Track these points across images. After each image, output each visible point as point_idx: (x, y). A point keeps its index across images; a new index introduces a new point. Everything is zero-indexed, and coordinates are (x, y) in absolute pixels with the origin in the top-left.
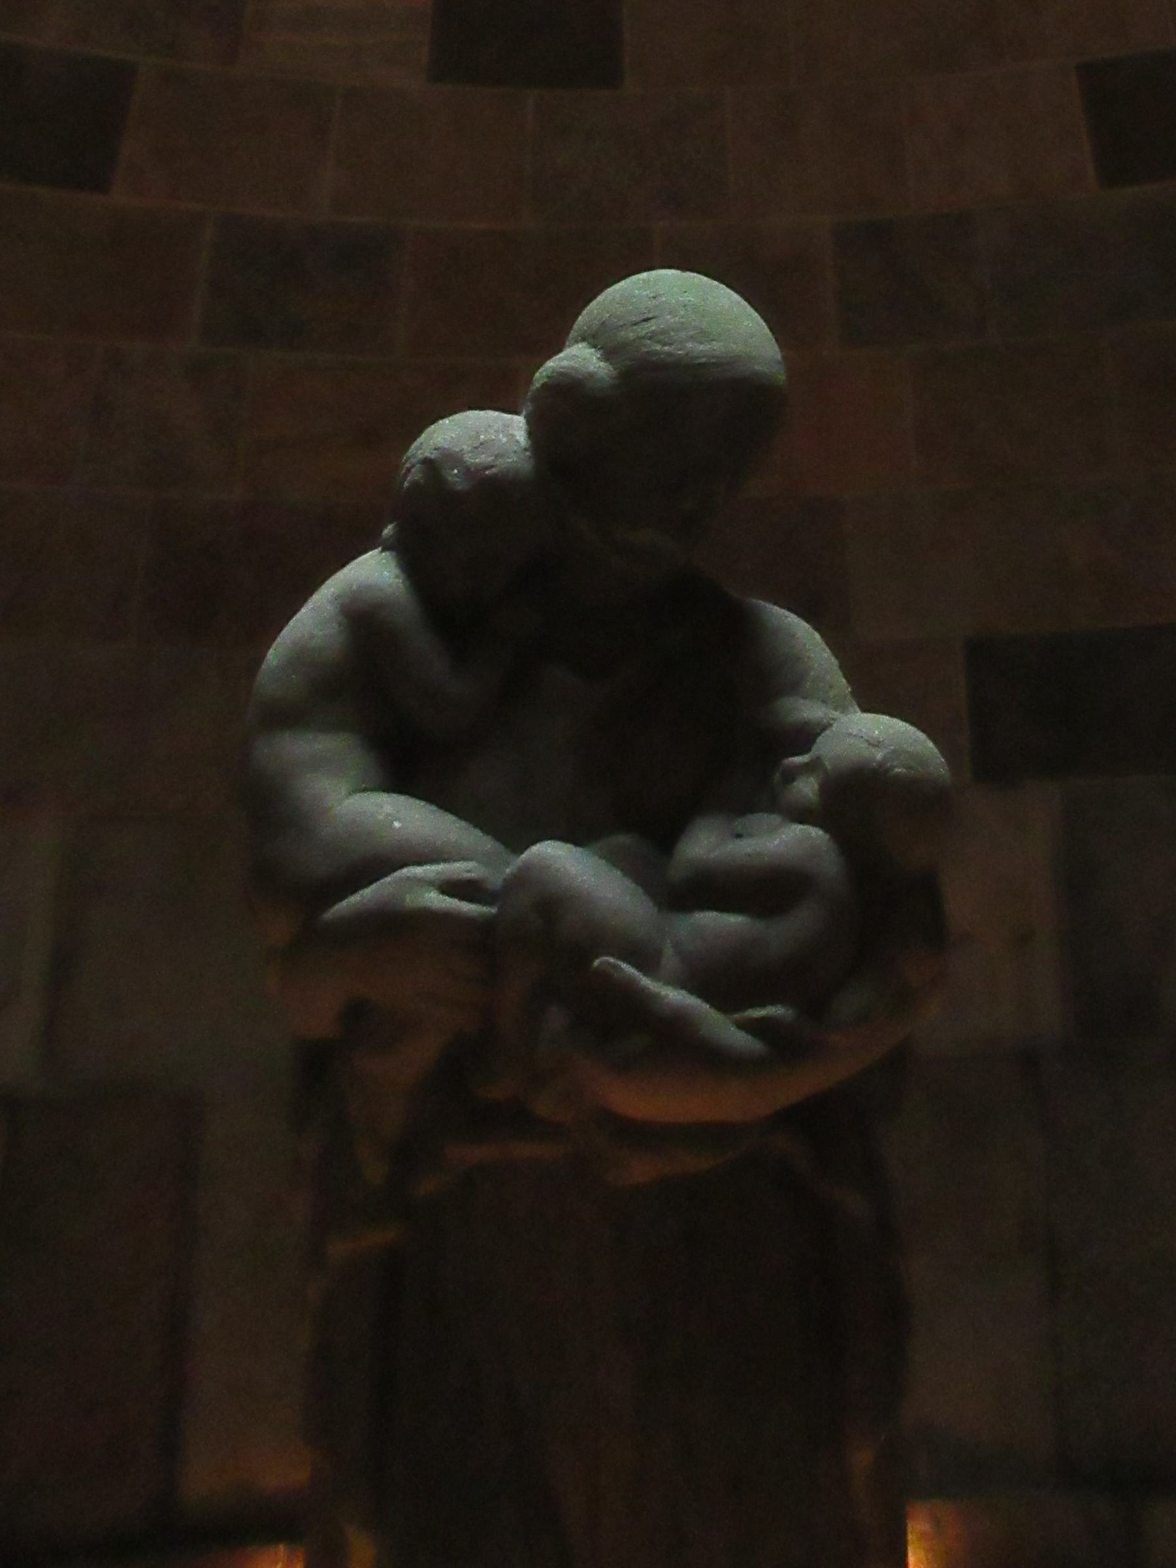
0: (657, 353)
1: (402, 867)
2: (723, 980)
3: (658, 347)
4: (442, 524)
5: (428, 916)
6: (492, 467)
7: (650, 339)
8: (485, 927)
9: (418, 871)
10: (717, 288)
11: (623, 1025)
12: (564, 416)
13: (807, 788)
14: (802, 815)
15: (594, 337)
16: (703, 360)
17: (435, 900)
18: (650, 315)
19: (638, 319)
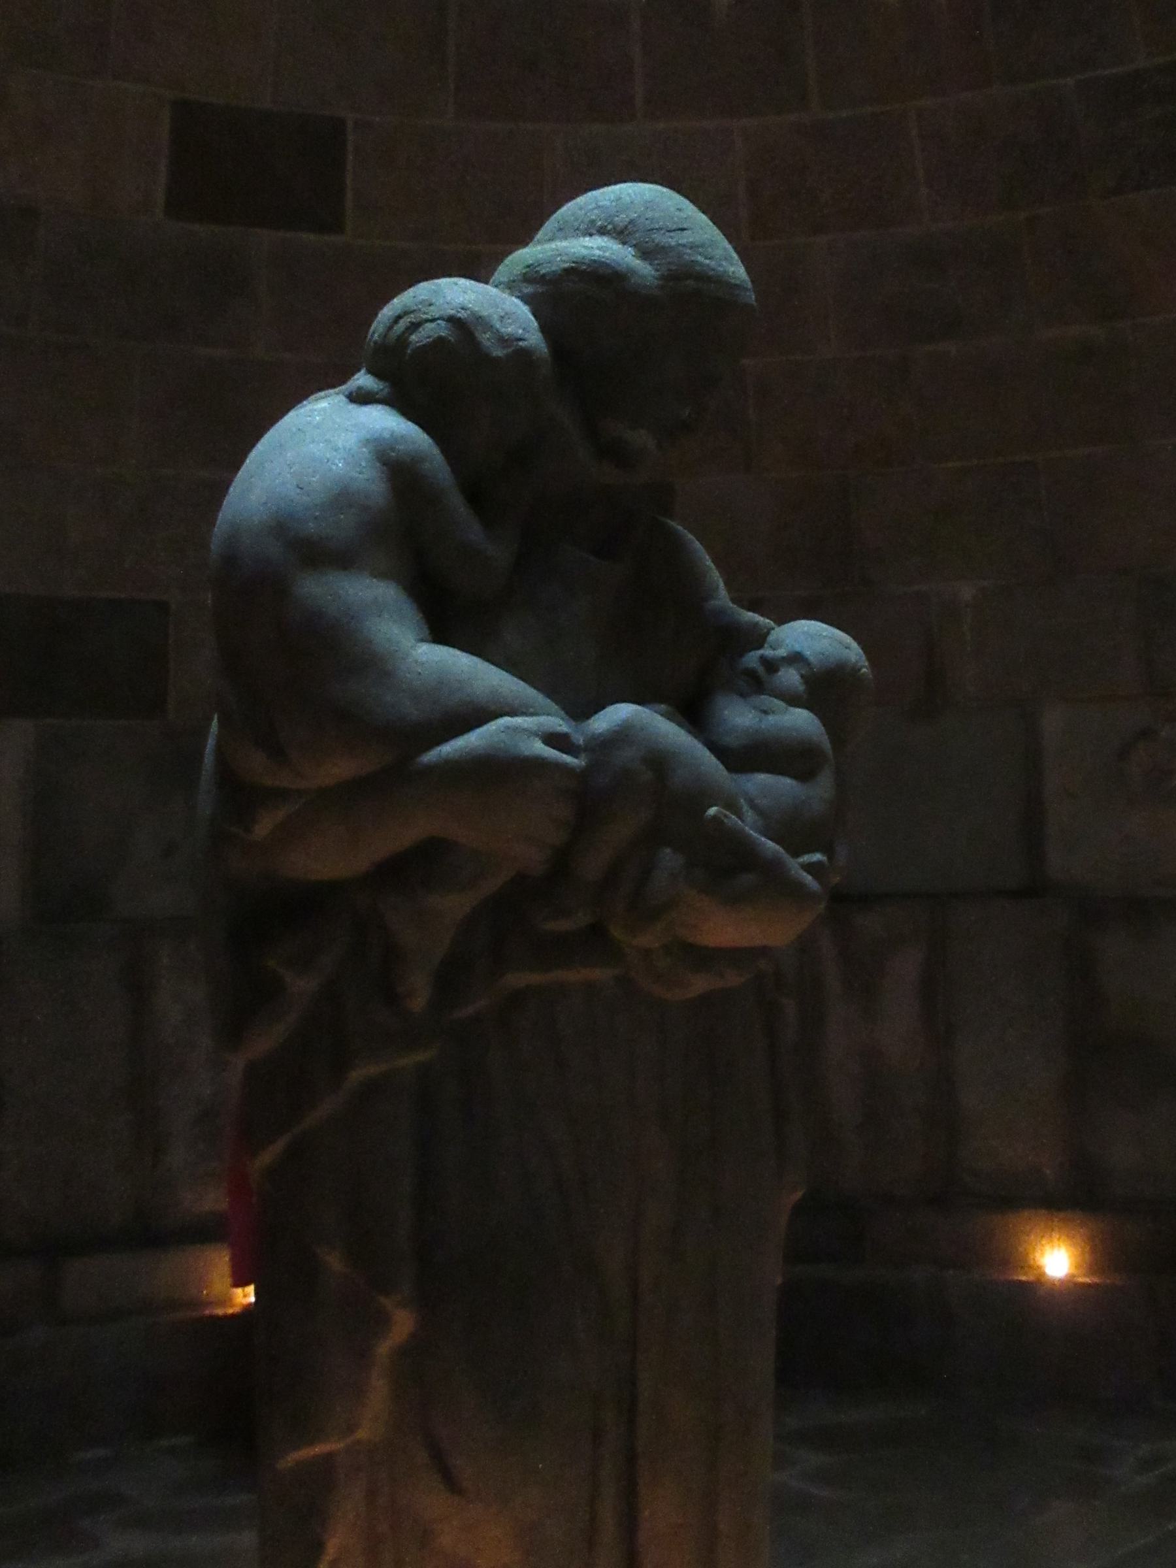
0: (701, 264)
1: (501, 716)
2: (796, 831)
3: (699, 258)
4: (427, 378)
5: (538, 764)
6: (520, 339)
7: (691, 248)
8: (582, 776)
9: (519, 720)
10: (670, 198)
11: (727, 865)
12: (568, 297)
13: (791, 677)
14: (793, 700)
15: (621, 232)
16: (738, 282)
17: (539, 748)
18: (685, 226)
19: (675, 227)
